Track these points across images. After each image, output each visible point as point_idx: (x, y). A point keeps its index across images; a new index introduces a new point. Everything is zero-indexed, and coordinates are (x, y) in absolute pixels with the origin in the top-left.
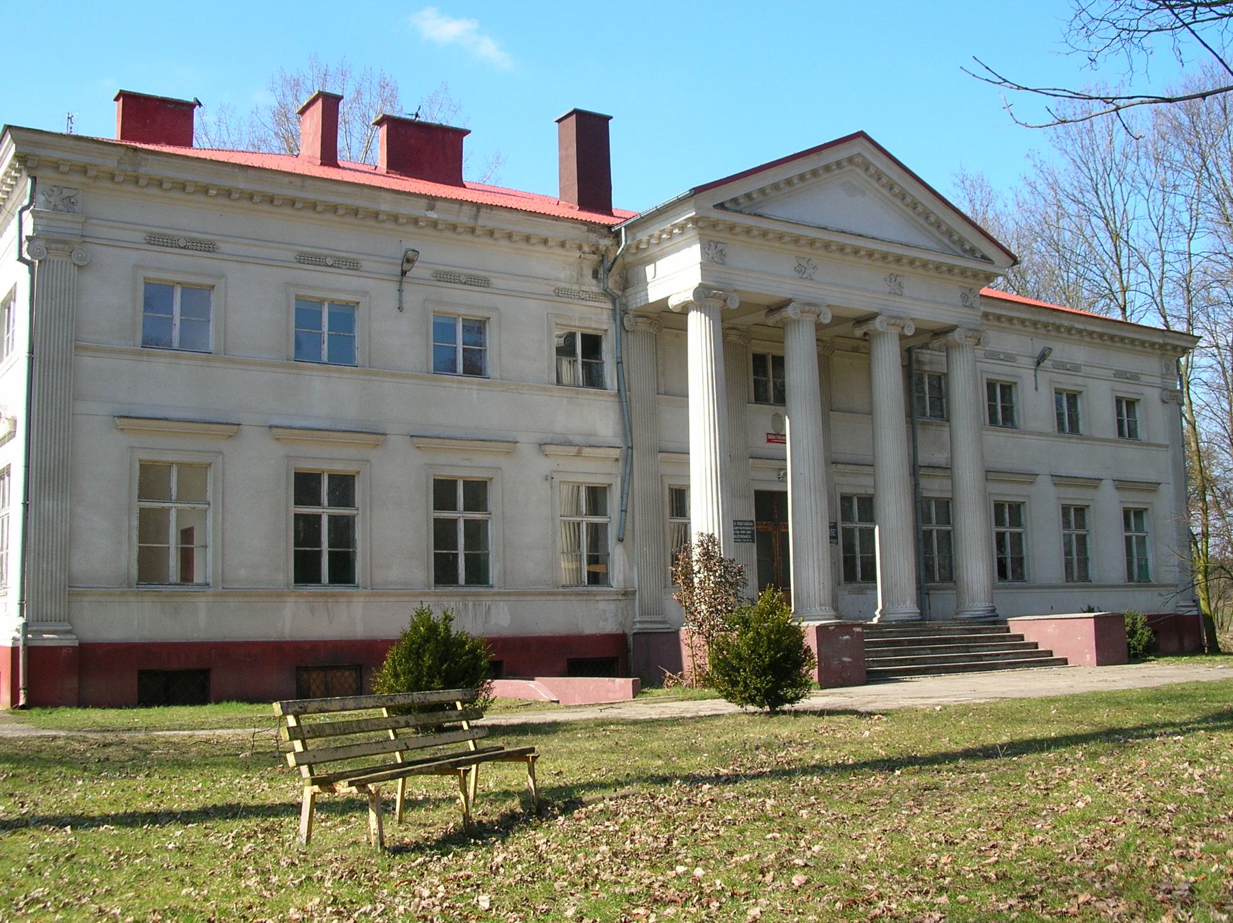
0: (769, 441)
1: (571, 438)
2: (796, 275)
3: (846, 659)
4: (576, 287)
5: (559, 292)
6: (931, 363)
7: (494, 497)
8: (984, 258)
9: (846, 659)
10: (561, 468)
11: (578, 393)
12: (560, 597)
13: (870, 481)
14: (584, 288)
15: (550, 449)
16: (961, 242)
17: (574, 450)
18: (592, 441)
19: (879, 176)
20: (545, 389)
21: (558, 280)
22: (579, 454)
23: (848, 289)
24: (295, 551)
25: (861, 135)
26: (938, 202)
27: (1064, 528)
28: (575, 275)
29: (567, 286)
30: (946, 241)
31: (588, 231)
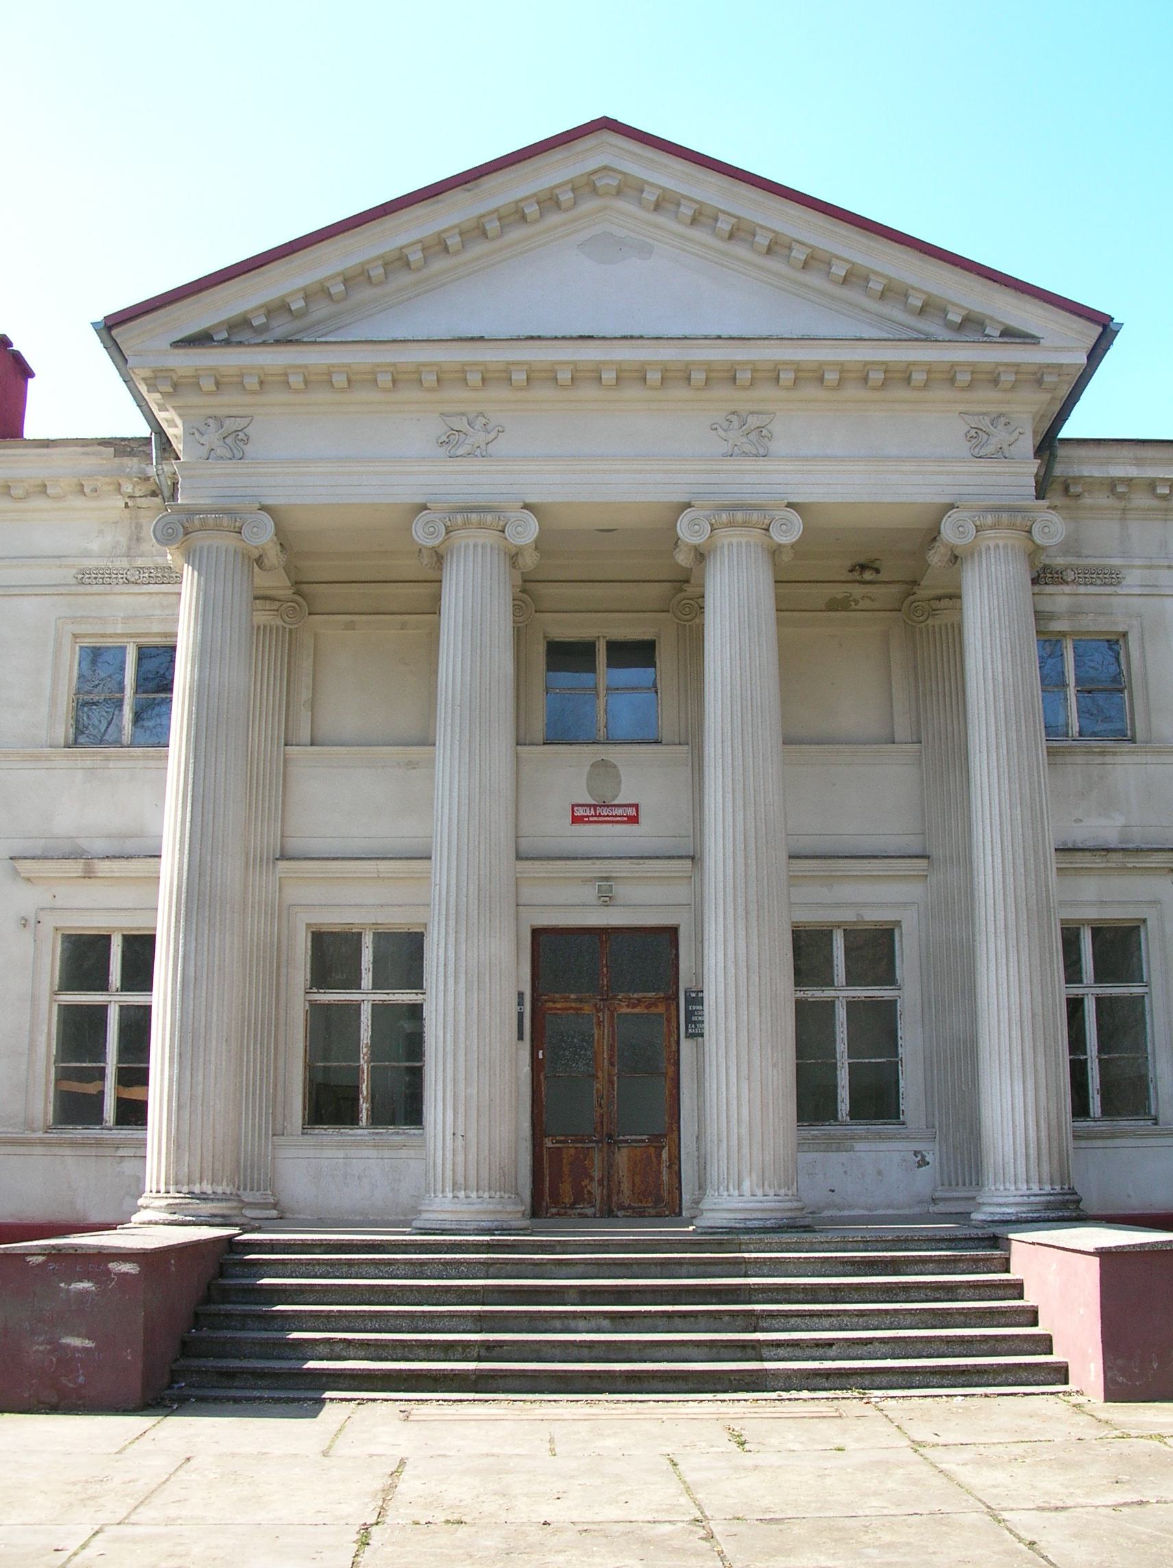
0: (576, 820)
1: (84, 843)
2: (442, 451)
3: (76, 1342)
4: (123, 563)
5: (86, 578)
6: (1074, 613)
7: (1156, 956)
8: (1010, 334)
9: (76, 1342)
10: (59, 903)
11: (107, 758)
12: (39, 1150)
13: (680, 893)
14: (139, 562)
15: (26, 866)
16: (930, 308)
17: (76, 867)
18: (130, 846)
19: (664, 203)
20: (37, 758)
21: (87, 554)
22: (89, 875)
23: (609, 465)
24: (104, 1061)
25: (606, 125)
26: (843, 229)
27: (1068, 980)
28: (123, 540)
29: (102, 563)
30: (898, 314)
31: (117, 454)
